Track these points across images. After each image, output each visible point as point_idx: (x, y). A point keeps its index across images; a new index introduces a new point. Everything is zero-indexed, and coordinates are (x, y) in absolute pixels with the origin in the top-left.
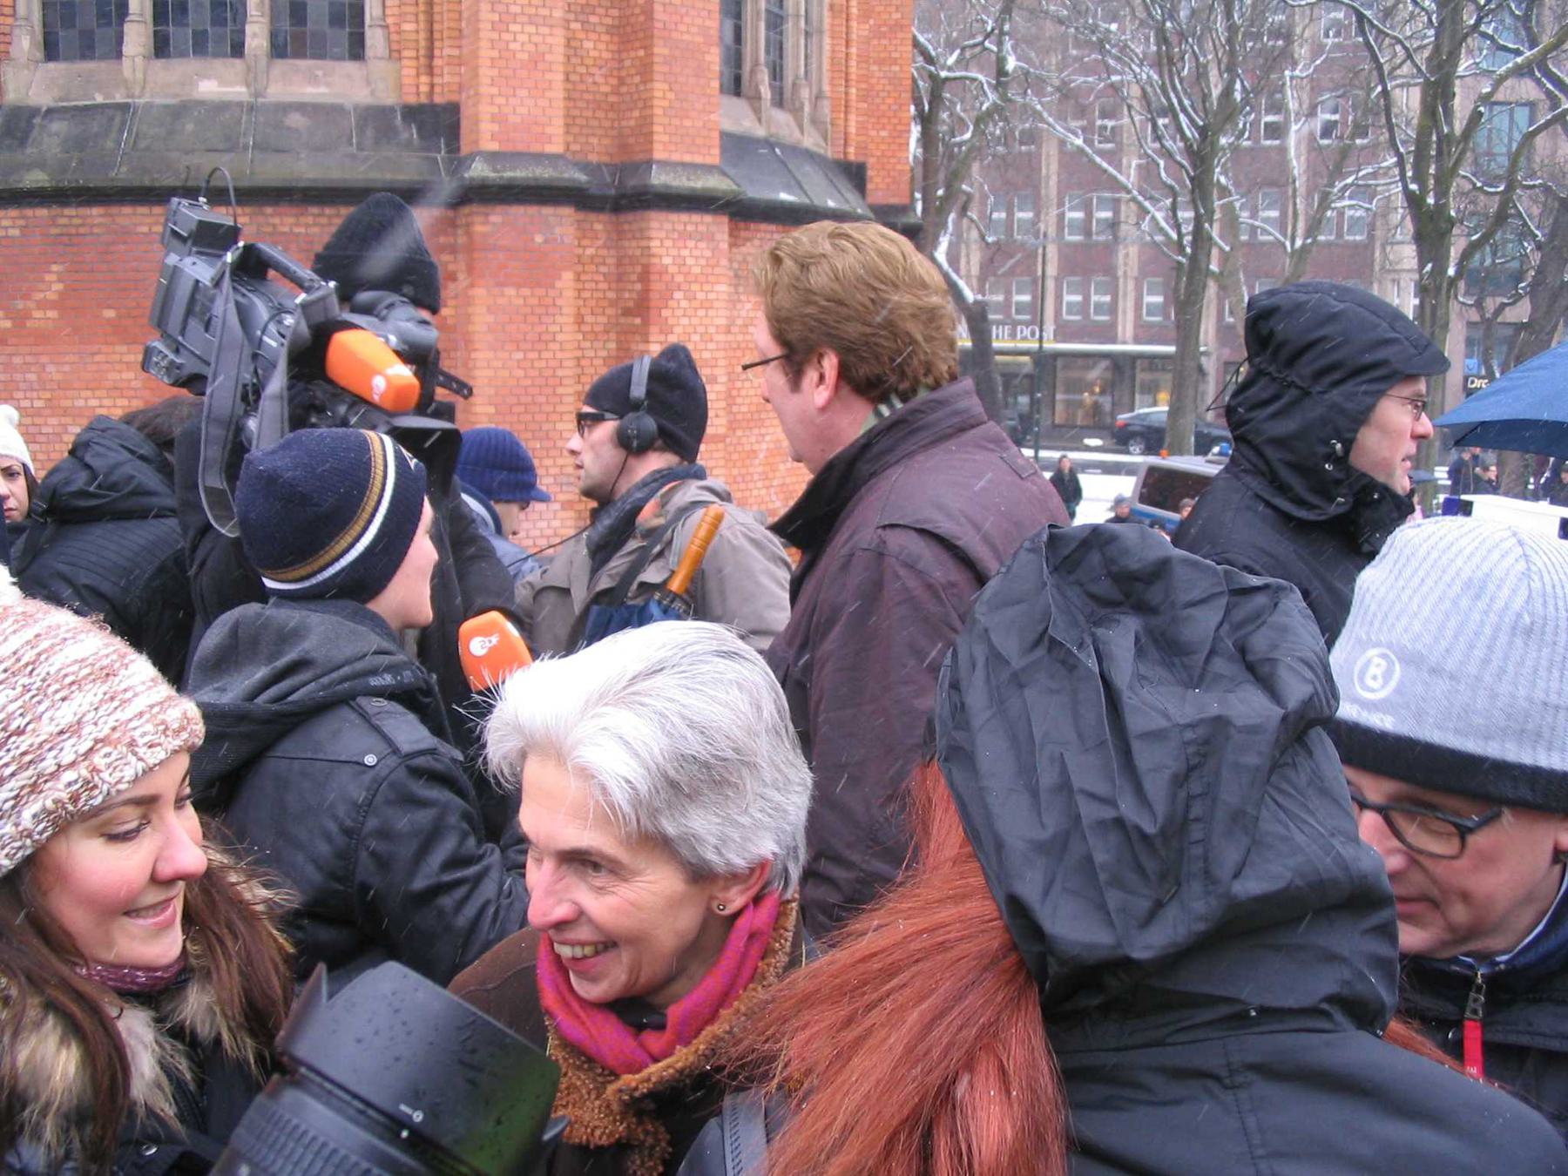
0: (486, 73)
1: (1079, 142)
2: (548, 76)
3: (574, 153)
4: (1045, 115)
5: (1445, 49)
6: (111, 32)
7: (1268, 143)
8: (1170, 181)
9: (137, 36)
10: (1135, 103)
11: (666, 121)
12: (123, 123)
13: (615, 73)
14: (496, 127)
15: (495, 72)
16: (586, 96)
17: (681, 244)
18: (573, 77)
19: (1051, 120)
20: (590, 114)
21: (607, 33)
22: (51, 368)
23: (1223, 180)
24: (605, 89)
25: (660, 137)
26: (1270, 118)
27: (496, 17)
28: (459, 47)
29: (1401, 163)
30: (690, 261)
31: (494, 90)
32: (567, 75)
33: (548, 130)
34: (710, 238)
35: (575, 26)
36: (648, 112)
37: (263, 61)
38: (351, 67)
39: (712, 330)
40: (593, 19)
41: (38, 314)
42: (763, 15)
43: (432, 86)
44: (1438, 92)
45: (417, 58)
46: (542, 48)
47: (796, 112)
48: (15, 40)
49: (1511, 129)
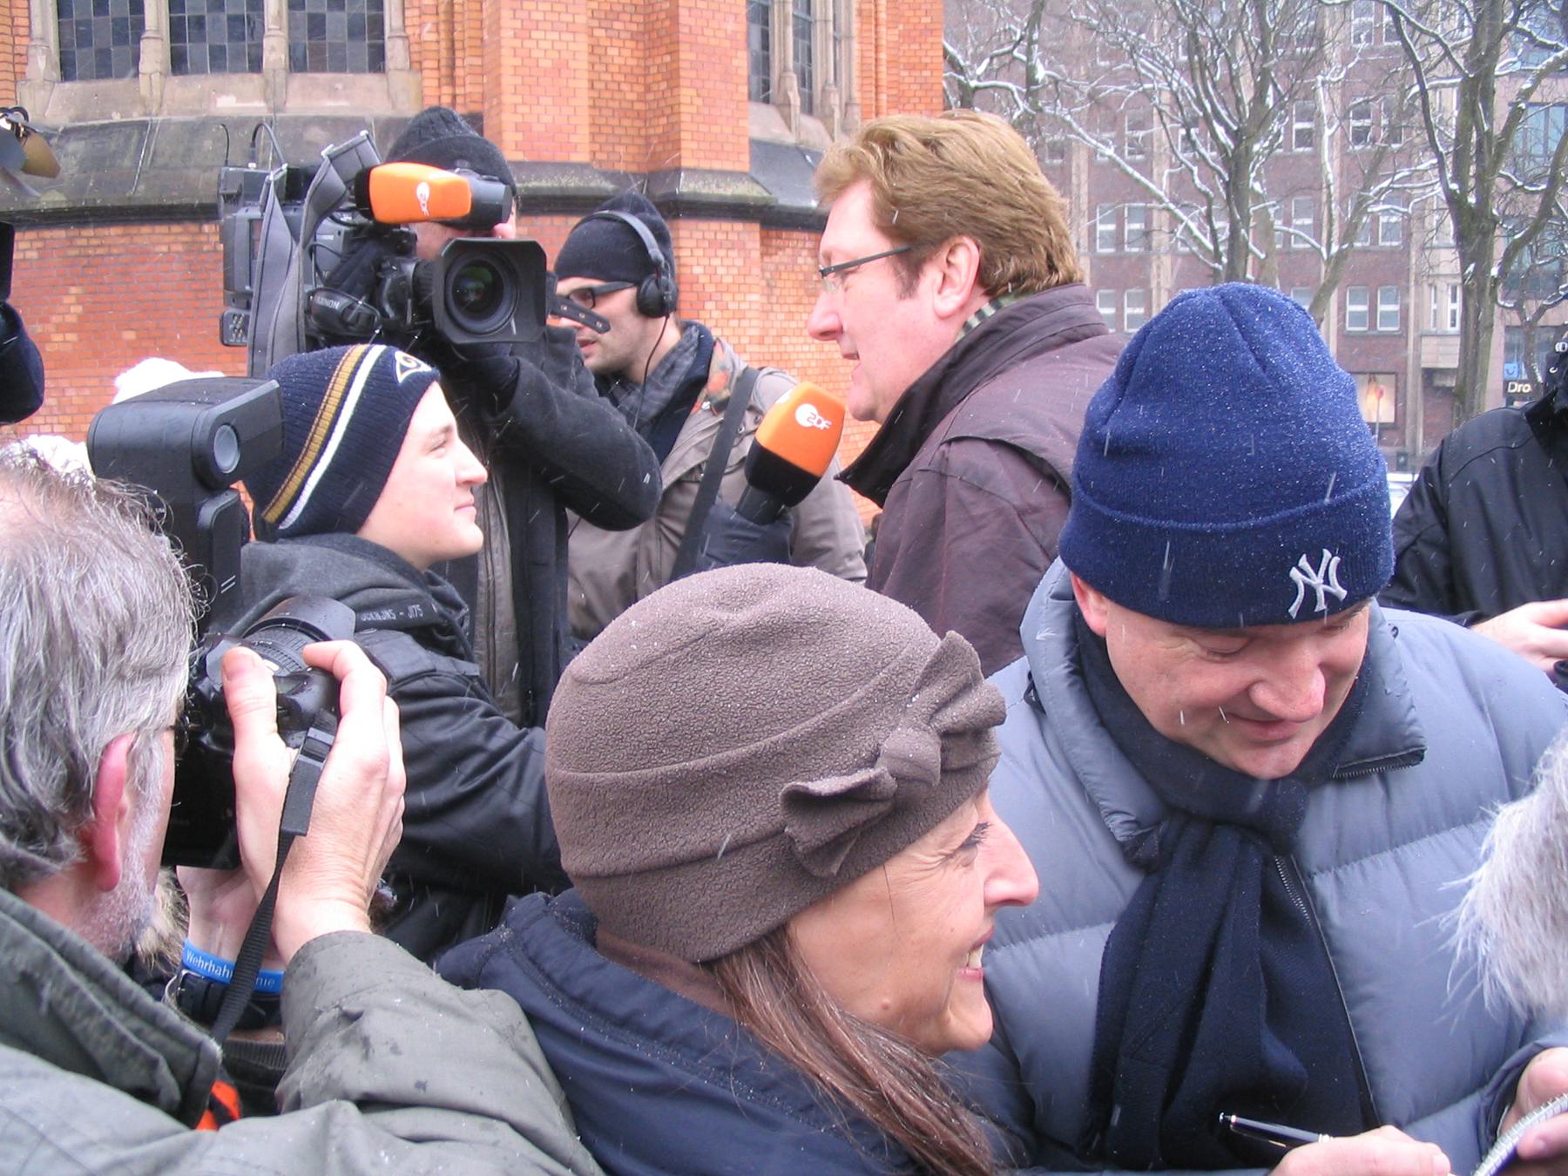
0: (508, 81)
1: (1110, 152)
2: (572, 84)
3: (600, 162)
4: (1075, 125)
5: (1484, 44)
6: (128, 49)
7: (1301, 150)
8: (1204, 188)
9: (154, 51)
10: (1166, 109)
11: (694, 127)
12: (141, 141)
13: (641, 80)
14: (519, 137)
15: (518, 81)
16: (611, 104)
17: (712, 252)
18: (598, 85)
19: (1081, 130)
20: (615, 122)
21: (632, 39)
22: (71, 392)
23: (1257, 187)
24: (631, 96)
25: (687, 145)
26: (1298, 126)
27: (518, 24)
28: (482, 56)
29: (1441, 166)
30: (721, 271)
31: (518, 99)
32: (592, 83)
33: (574, 139)
34: (741, 246)
35: (599, 33)
36: (674, 119)
37: (281, 77)
38: (371, 79)
39: (745, 340)
40: (618, 25)
41: (58, 338)
42: (791, 19)
43: (454, 96)
44: (1477, 90)
45: (439, 68)
46: (565, 55)
47: (826, 118)
48: (31, 59)
49: (1546, 128)
